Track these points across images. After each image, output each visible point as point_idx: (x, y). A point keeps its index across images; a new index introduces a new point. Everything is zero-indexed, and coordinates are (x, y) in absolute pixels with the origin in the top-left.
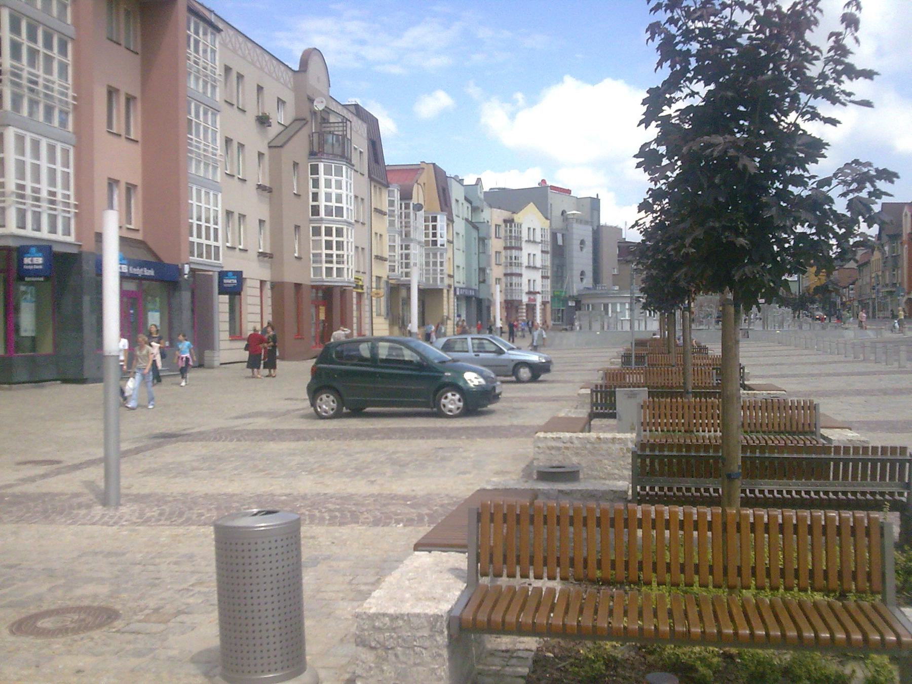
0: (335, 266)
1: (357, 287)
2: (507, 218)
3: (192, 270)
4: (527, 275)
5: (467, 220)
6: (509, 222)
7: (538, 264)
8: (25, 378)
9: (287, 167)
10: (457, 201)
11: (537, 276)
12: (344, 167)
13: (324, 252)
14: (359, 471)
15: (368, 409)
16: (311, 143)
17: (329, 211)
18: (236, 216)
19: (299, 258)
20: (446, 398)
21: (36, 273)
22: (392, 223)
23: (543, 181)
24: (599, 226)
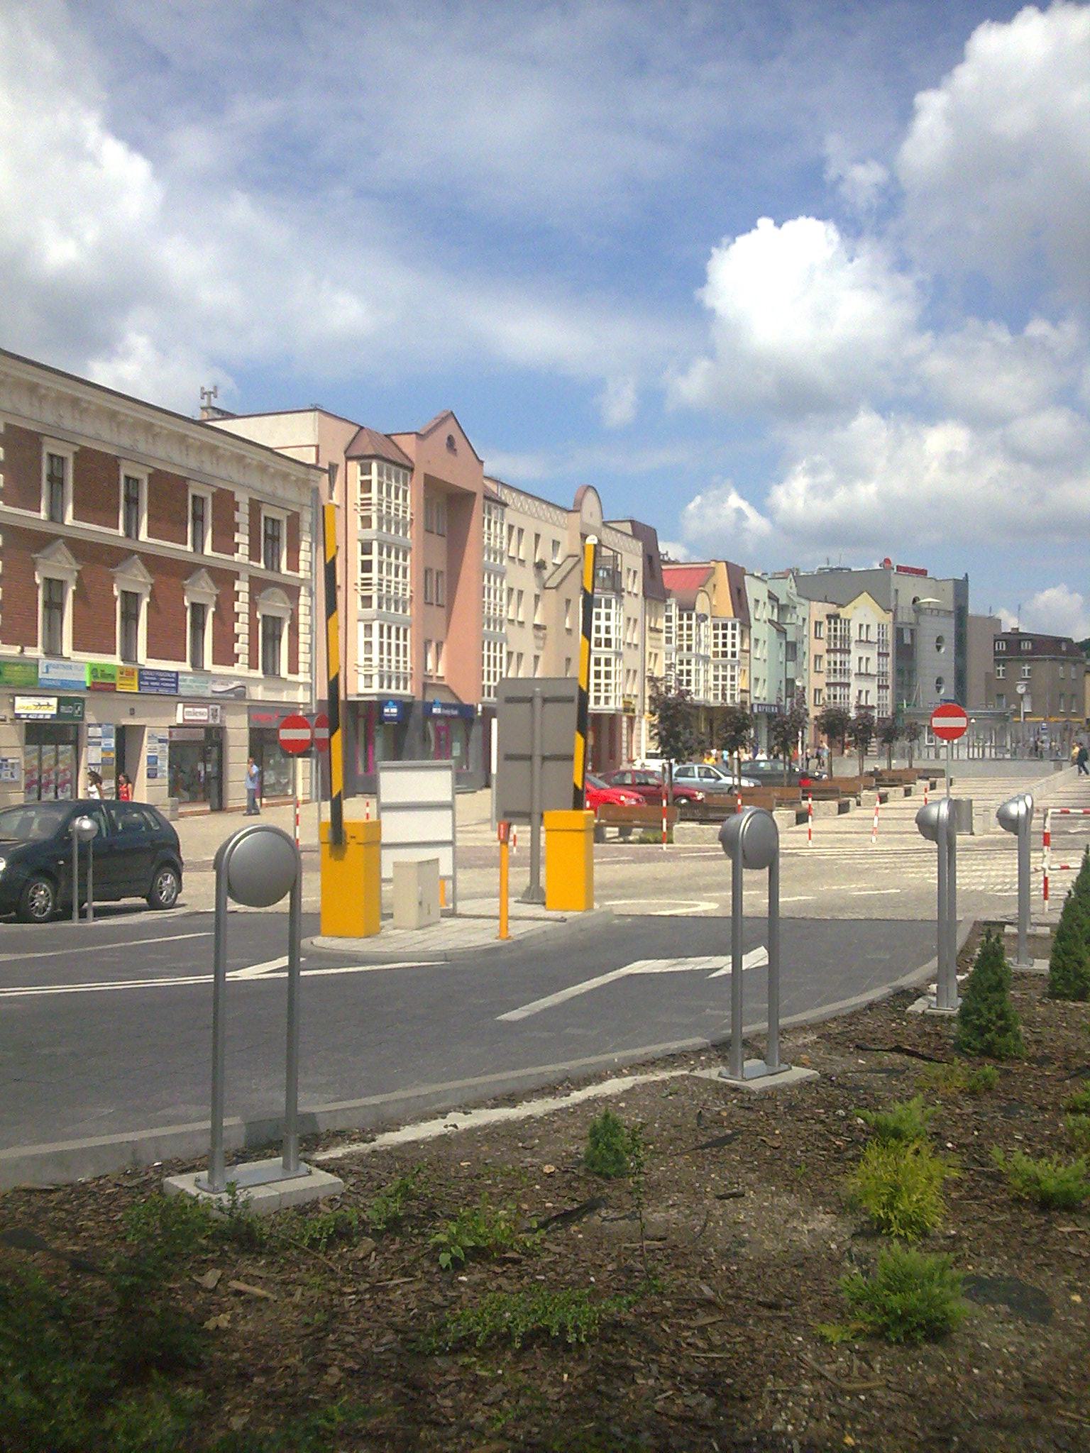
1: (626, 710)
3: (483, 708)
6: (832, 617)
10: (757, 601)
11: (872, 686)
12: (613, 601)
18: (515, 656)
21: (391, 719)
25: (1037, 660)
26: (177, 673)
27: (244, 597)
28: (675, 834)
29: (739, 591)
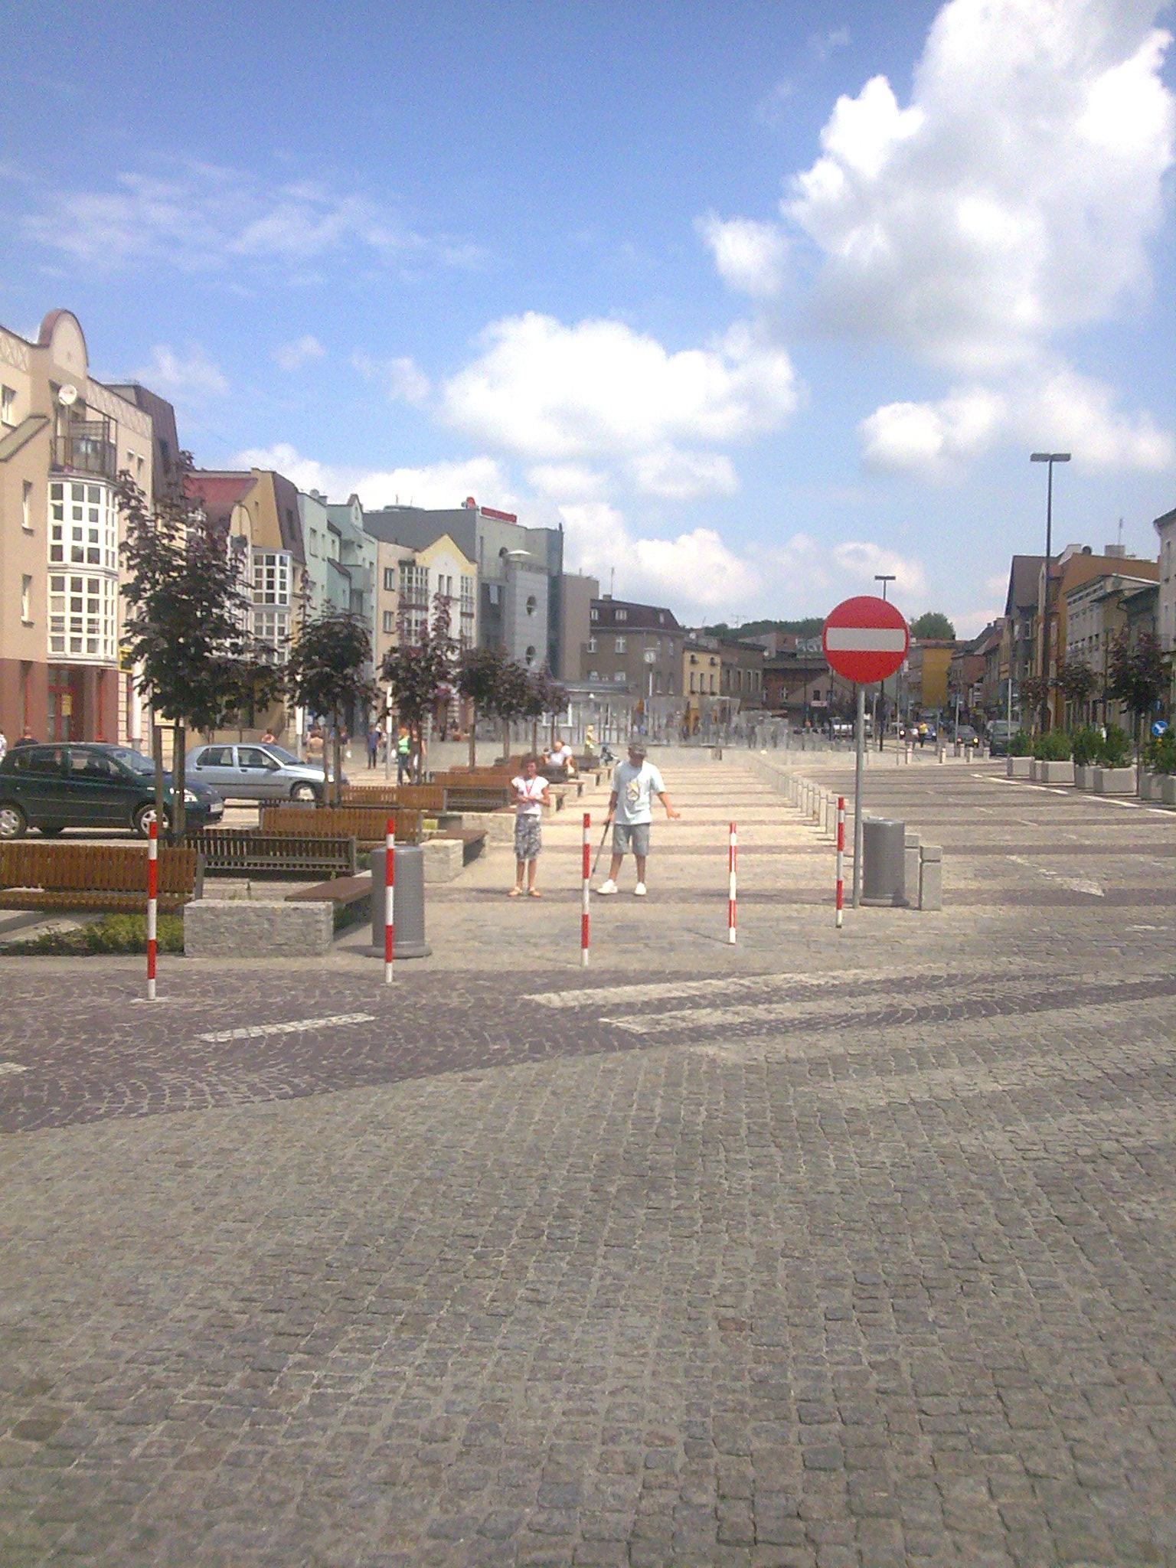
0: (85, 636)
1: (687, 1428)
6: (407, 564)
10: (314, 531)
12: (103, 491)
15: (67, 830)
16: (54, 452)
17: (78, 557)
19: (28, 624)
23: (471, 500)
25: (632, 632)
28: (189, 927)
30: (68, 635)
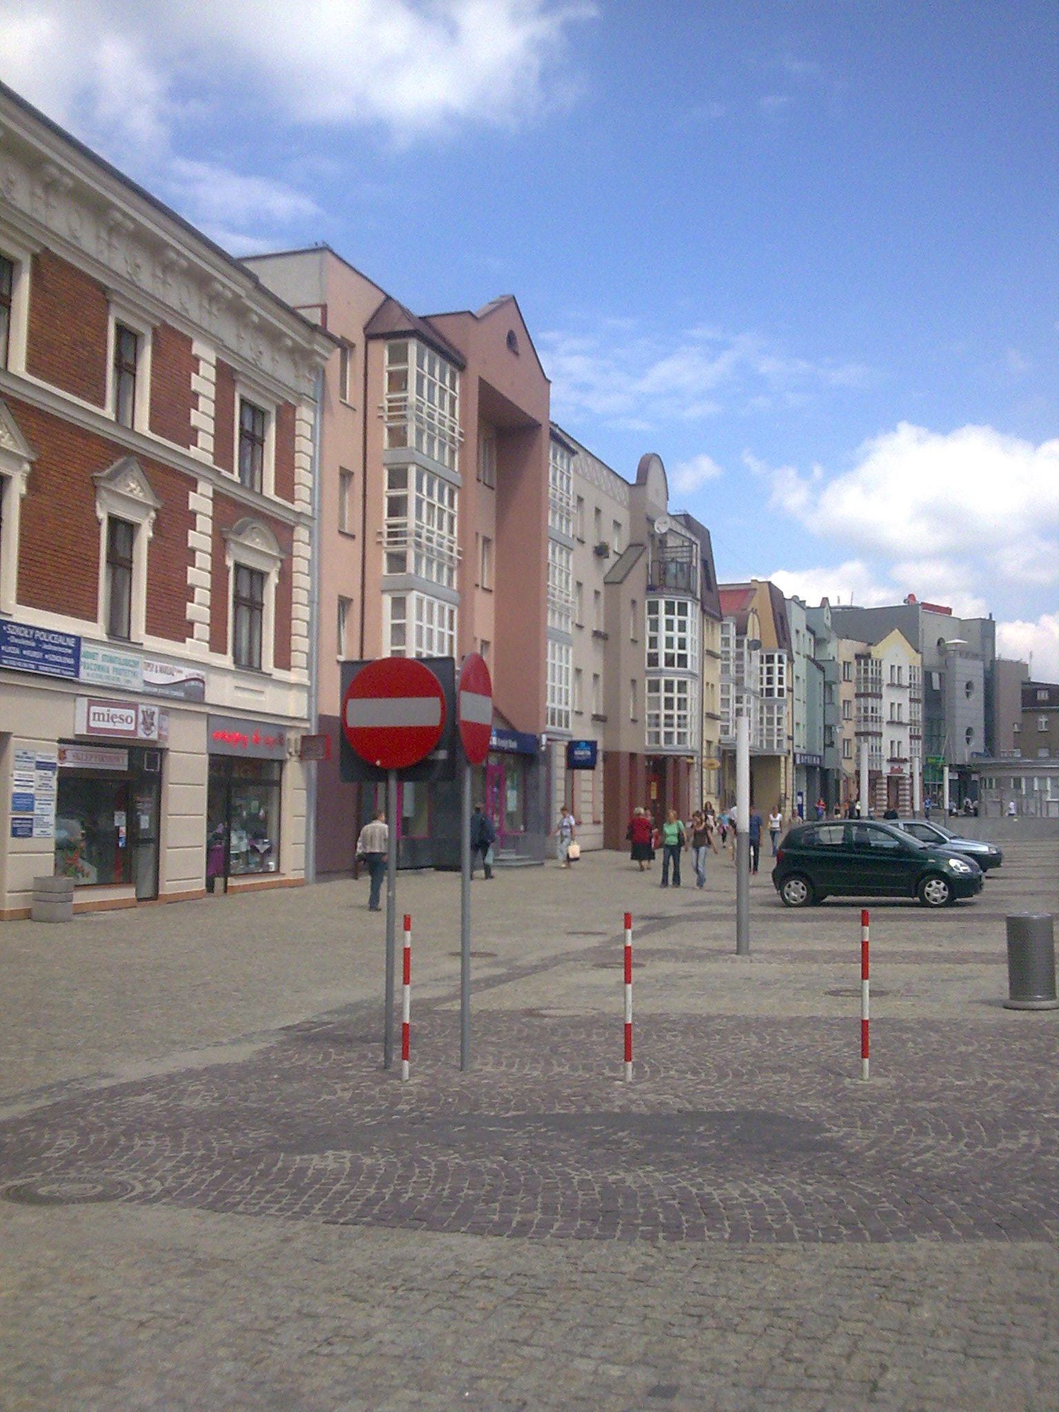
0: (675, 730)
2: (859, 652)
4: (889, 734)
5: (808, 657)
6: (862, 657)
7: (906, 719)
8: (408, 865)
9: (626, 606)
11: (903, 735)
13: (663, 712)
14: (909, 939)
17: (669, 661)
19: (634, 721)
20: (930, 886)
22: (725, 668)
24: (993, 661)
26: (78, 639)
27: (204, 524)
29: (782, 618)
30: (663, 730)
